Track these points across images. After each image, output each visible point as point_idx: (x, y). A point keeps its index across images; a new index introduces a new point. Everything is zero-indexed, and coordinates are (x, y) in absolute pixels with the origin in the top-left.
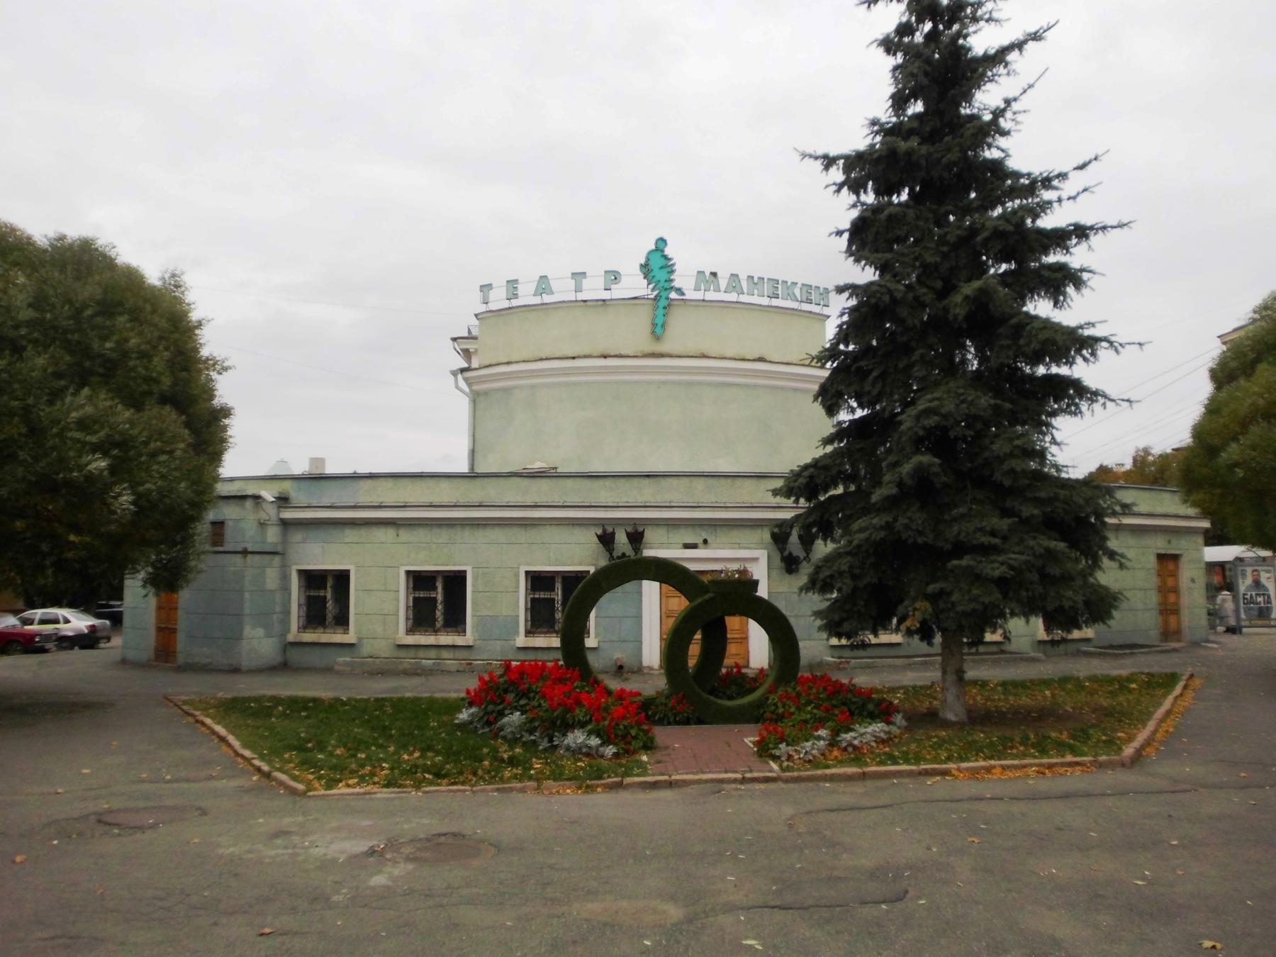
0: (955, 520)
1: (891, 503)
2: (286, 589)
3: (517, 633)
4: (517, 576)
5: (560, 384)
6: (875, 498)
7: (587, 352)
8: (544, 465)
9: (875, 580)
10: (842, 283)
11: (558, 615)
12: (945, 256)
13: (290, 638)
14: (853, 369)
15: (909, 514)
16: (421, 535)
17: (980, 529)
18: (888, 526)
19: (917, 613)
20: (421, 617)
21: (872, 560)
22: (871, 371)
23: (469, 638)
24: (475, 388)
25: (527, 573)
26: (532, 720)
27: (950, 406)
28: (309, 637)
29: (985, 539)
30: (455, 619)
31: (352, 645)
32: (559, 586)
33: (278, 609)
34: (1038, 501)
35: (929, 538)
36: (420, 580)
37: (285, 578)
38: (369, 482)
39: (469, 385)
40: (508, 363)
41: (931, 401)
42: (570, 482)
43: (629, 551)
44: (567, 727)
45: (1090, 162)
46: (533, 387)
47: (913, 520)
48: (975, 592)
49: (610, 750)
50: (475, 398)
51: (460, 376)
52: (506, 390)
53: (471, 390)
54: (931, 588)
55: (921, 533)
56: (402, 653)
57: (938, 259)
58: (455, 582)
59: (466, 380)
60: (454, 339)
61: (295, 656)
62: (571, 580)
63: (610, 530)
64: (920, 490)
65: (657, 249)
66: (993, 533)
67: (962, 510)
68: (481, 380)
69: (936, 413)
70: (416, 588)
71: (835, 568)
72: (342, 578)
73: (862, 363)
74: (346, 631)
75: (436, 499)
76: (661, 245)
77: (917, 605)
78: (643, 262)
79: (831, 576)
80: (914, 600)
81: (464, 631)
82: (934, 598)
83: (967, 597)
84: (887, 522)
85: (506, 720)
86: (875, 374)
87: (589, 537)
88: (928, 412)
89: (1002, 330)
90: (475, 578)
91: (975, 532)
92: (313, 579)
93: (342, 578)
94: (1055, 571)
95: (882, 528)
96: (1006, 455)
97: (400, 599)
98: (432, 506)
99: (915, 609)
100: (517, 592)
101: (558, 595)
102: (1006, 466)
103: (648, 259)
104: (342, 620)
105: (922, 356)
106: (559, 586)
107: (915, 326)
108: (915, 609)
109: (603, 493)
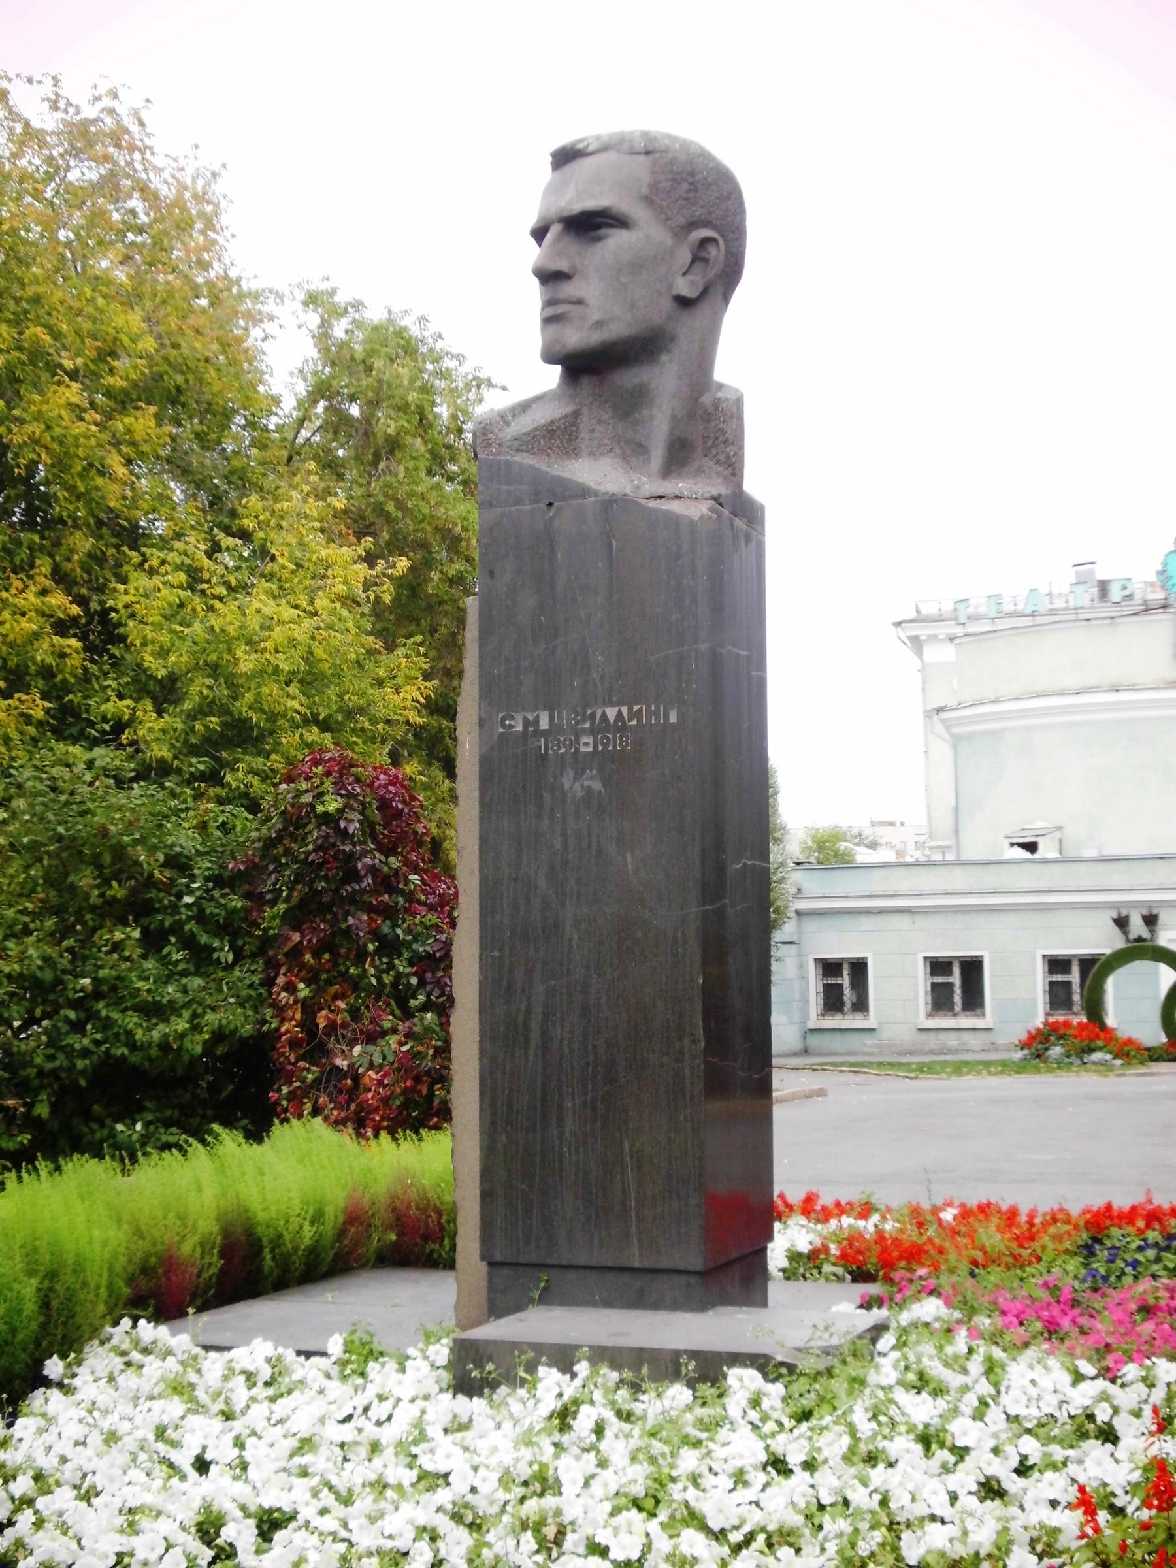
2: (803, 978)
4: (1034, 959)
8: (1046, 825)
11: (1076, 997)
13: (811, 1025)
16: (937, 921)
20: (940, 1000)
24: (954, 730)
28: (831, 1022)
30: (973, 999)
31: (873, 1030)
32: (956, 970)
33: (797, 997)
36: (938, 966)
37: (802, 966)
38: (882, 872)
39: (948, 728)
40: (994, 702)
42: (1083, 867)
43: (1146, 934)
44: (1092, 1050)
49: (1118, 1062)
50: (957, 742)
51: (935, 718)
52: (994, 733)
53: (953, 736)
56: (924, 1037)
58: (972, 968)
59: (943, 721)
60: (898, 624)
61: (814, 1041)
62: (1087, 963)
63: (1124, 913)
68: (961, 721)
70: (933, 974)
72: (859, 968)
74: (866, 1017)
75: (950, 887)
78: (1160, 568)
81: (983, 1015)
87: (1105, 922)
90: (992, 962)
92: (830, 968)
93: (859, 968)
97: (921, 982)
101: (1075, 977)
103: (1165, 564)
104: (861, 1006)
106: (846, 972)
109: (1116, 876)
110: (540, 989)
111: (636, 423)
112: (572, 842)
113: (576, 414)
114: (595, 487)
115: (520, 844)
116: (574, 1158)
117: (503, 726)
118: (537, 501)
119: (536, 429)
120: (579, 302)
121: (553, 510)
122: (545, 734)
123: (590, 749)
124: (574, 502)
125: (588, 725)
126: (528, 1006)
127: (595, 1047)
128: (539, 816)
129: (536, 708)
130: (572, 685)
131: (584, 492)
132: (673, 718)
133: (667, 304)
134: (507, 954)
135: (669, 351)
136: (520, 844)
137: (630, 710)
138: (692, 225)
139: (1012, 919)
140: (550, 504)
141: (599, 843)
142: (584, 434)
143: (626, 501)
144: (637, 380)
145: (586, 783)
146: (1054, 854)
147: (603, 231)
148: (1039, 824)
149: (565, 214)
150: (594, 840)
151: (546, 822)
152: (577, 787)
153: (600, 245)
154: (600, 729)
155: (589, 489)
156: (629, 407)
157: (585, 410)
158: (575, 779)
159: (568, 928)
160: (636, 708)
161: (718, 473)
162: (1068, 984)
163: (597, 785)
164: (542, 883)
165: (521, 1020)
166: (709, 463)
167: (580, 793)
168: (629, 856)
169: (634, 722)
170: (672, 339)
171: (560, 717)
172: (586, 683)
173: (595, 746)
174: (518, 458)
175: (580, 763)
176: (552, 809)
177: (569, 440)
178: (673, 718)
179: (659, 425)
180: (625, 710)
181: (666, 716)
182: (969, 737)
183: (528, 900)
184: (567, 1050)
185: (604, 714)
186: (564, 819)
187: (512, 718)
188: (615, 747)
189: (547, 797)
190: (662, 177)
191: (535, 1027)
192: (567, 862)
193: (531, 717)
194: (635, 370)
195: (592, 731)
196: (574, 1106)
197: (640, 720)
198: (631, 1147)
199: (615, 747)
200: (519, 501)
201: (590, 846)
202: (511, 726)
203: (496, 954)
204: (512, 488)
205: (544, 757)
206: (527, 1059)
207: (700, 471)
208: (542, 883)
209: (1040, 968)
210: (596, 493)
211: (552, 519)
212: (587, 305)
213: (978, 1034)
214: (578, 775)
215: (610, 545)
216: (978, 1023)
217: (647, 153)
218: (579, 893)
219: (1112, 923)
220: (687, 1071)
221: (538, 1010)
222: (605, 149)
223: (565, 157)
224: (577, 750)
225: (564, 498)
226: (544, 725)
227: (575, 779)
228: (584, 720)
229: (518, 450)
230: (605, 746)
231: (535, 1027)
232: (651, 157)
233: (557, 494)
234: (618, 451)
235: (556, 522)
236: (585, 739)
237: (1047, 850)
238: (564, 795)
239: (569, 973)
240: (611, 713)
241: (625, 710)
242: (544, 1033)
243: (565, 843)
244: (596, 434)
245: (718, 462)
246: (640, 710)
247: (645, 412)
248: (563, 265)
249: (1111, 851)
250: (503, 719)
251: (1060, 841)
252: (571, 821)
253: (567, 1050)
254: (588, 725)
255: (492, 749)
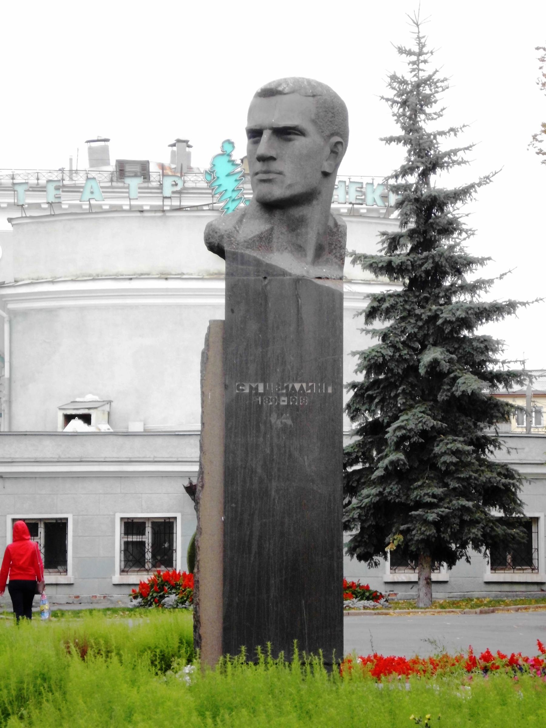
0: (416, 488)
1: (382, 480)
3: (114, 573)
5: (115, 307)
6: (373, 477)
7: (143, 268)
8: (96, 398)
9: (374, 523)
10: (354, 350)
12: (420, 328)
14: (365, 396)
15: (391, 486)
16: (26, 487)
17: (427, 494)
18: (381, 494)
19: (395, 541)
21: (372, 511)
22: (375, 398)
23: (70, 576)
24: (11, 306)
25: (122, 519)
26: (182, 598)
27: (411, 426)
29: (428, 499)
32: (149, 529)
34: (459, 480)
35: (403, 499)
40: (53, 282)
41: (403, 421)
42: (159, 441)
45: (506, 274)
46: (82, 308)
47: (393, 488)
48: (423, 529)
52: (50, 311)
54: (402, 527)
55: (398, 496)
57: (416, 330)
64: (394, 473)
65: (224, 154)
66: (434, 496)
67: (419, 483)
69: (405, 429)
71: (351, 516)
73: (370, 392)
75: (39, 455)
76: (228, 148)
77: (395, 537)
79: (349, 521)
80: (394, 534)
81: (66, 571)
82: (404, 533)
83: (419, 532)
84: (380, 492)
85: (166, 599)
86: (377, 400)
88: (400, 428)
89: (446, 380)
91: (424, 495)
94: (467, 518)
95: (377, 495)
96: (442, 453)
98: (37, 462)
99: (394, 539)
100: (113, 536)
102: (443, 459)
105: (404, 390)
106: (149, 529)
107: (398, 373)
108: (394, 539)
110: (257, 524)
111: (298, 235)
112: (275, 450)
113: (272, 229)
114: (289, 271)
115: (247, 449)
116: (275, 609)
117: (239, 389)
118: (258, 276)
119: (254, 237)
120: (280, 173)
121: (266, 282)
122: (262, 395)
123: (286, 403)
124: (278, 278)
125: (284, 391)
126: (251, 532)
127: (287, 553)
128: (257, 437)
129: (256, 381)
130: (276, 371)
131: (284, 273)
132: (330, 390)
133: (319, 175)
134: (240, 505)
135: (317, 199)
136: (247, 449)
137: (307, 385)
138: (332, 135)
139: (97, 486)
140: (265, 278)
141: (290, 451)
142: (275, 240)
143: (307, 280)
144: (301, 214)
145: (283, 421)
146: (105, 427)
147: (292, 137)
148: (89, 397)
149: (274, 126)
150: (287, 450)
151: (261, 439)
152: (279, 422)
153: (291, 143)
154: (291, 394)
155: (286, 271)
156: (296, 226)
157: (276, 227)
158: (278, 418)
159: (273, 493)
160: (310, 384)
161: (336, 263)
162: (143, 544)
163: (289, 422)
164: (259, 470)
165: (247, 539)
166: (331, 257)
167: (280, 426)
168: (306, 457)
169: (309, 391)
170: (319, 193)
171: (270, 386)
172: (284, 370)
173: (288, 402)
174: (248, 252)
175: (281, 411)
176: (265, 434)
177: (269, 243)
178: (330, 390)
179: (311, 236)
180: (304, 385)
181: (326, 389)
182: (25, 313)
183: (251, 478)
184: (272, 554)
185: (293, 387)
186: (272, 438)
187: (243, 385)
188: (299, 403)
189: (262, 427)
190: (320, 111)
191: (255, 542)
192: (273, 460)
193: (254, 385)
194: (301, 208)
195: (288, 395)
196: (275, 582)
197: (312, 390)
198: (306, 602)
199: (299, 403)
200: (248, 274)
201: (285, 452)
202: (243, 390)
203: (234, 505)
204: (244, 267)
205: (260, 407)
206: (250, 560)
207: (327, 261)
208: (259, 470)
209: (118, 529)
210: (290, 275)
211: (266, 285)
212: (284, 175)
213: (59, 589)
214: (280, 415)
215: (298, 301)
216: (61, 579)
217: (314, 96)
218: (279, 476)
219: (184, 490)
220: (335, 565)
221: (256, 534)
222: (293, 92)
223: (268, 93)
224: (279, 404)
225: (273, 275)
226: (261, 390)
227: (278, 418)
228: (283, 389)
229: (247, 248)
230: (294, 402)
231: (255, 542)
232: (316, 98)
233: (269, 272)
234: (289, 249)
235: (268, 287)
236: (283, 398)
237: (99, 424)
238: (271, 425)
239: (273, 516)
240: (297, 386)
241: (304, 385)
242: (260, 546)
243: (272, 451)
244: (280, 240)
245: (336, 256)
246: (313, 385)
247: (303, 230)
248: (273, 153)
249: (155, 425)
250: (238, 386)
251: (109, 413)
252: (275, 440)
253: (272, 554)
254: (284, 391)
255: (233, 400)
